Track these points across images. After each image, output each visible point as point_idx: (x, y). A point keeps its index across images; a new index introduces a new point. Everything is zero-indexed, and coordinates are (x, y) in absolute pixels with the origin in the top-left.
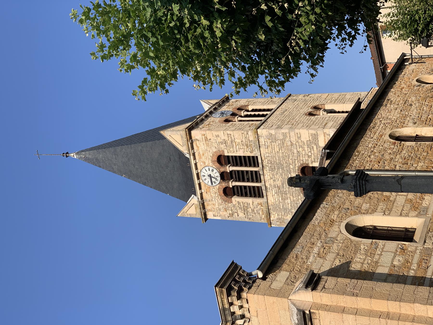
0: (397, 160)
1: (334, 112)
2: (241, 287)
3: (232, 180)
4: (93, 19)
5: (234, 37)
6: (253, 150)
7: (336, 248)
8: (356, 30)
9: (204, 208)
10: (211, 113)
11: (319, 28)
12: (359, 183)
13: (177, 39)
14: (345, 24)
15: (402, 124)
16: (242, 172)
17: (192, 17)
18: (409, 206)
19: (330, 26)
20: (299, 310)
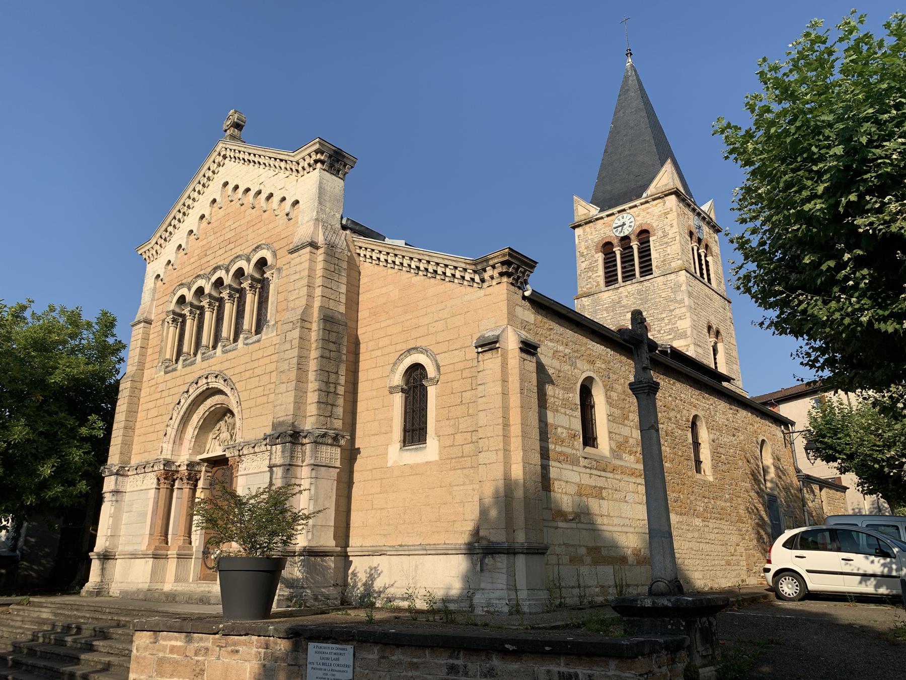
0: (670, 424)
1: (715, 354)
4: (812, 49)
5: (804, 226)
8: (822, 368)
9: (586, 223)
10: (699, 214)
11: (824, 324)
13: (796, 158)
14: (829, 355)
16: (633, 260)
17: (826, 172)
18: (621, 440)
19: (825, 338)
20: (498, 336)
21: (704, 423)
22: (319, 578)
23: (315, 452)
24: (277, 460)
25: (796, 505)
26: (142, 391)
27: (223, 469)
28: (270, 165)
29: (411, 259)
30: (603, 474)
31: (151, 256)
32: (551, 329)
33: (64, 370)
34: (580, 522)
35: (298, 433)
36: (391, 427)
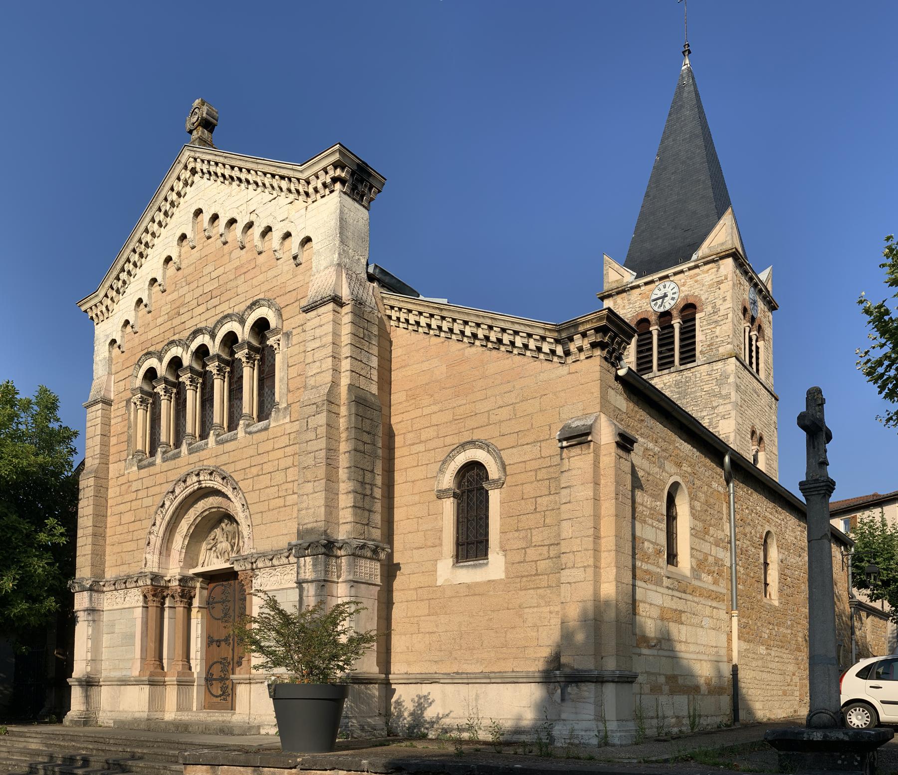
2: (607, 347)
3: (659, 329)
6: (704, 354)
7: (655, 472)
9: (618, 293)
10: (756, 285)
12: (823, 486)
15: (781, 546)
16: (673, 343)
18: (701, 557)
20: (591, 426)
21: (775, 540)
22: (364, 708)
23: (352, 567)
24: (308, 574)
25: (845, 633)
26: (110, 490)
27: (223, 585)
28: (264, 185)
29: (466, 323)
30: (683, 595)
31: (99, 313)
32: (642, 421)
33: (10, 461)
34: (661, 649)
35: (332, 543)
36: (440, 539)
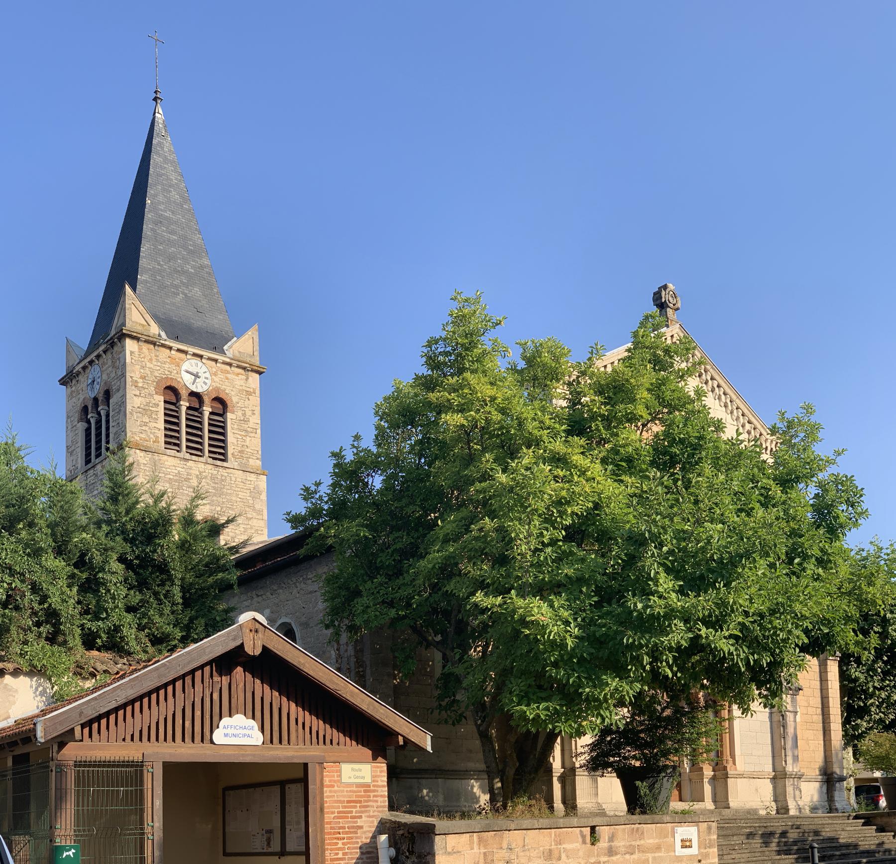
9: (147, 341)
